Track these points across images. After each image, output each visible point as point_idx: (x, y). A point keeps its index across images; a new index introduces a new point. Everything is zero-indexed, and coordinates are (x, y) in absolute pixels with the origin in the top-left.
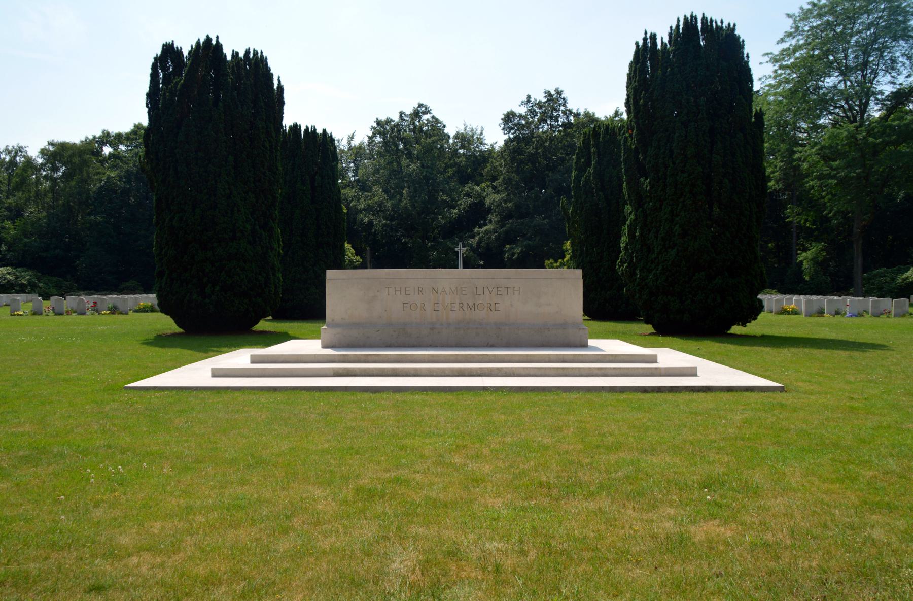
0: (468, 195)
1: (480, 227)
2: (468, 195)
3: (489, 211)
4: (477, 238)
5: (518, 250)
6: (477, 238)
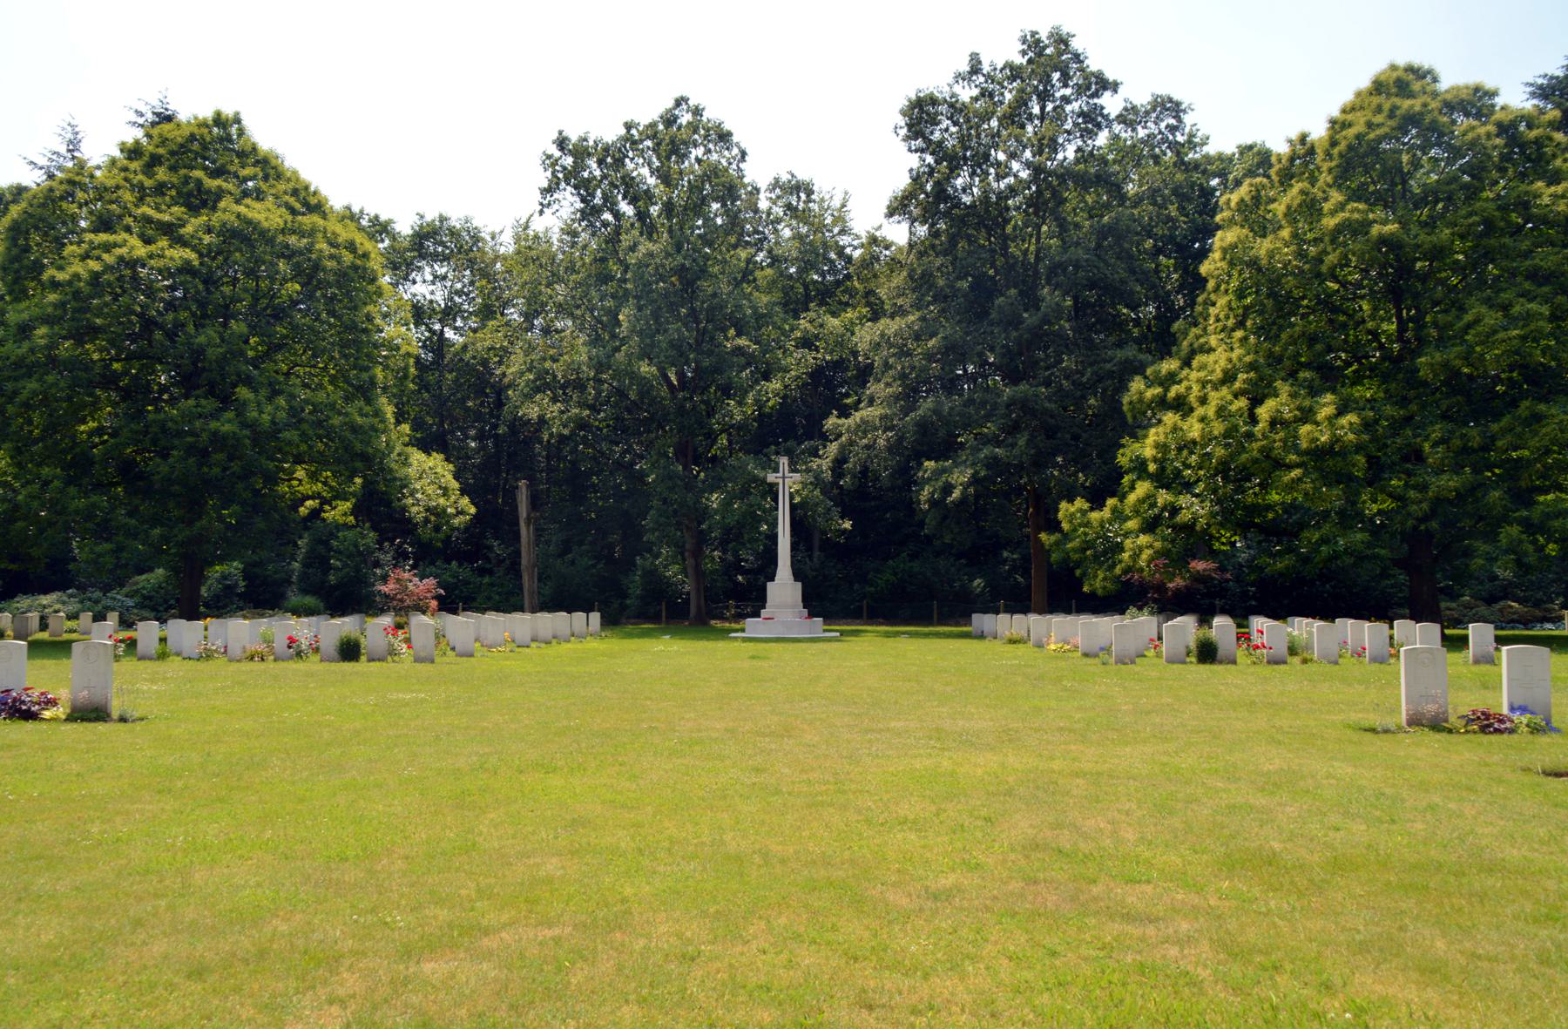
0: (807, 343)
1: (844, 413)
2: (807, 343)
3: (865, 374)
4: (833, 448)
5: (960, 477)
6: (833, 448)
